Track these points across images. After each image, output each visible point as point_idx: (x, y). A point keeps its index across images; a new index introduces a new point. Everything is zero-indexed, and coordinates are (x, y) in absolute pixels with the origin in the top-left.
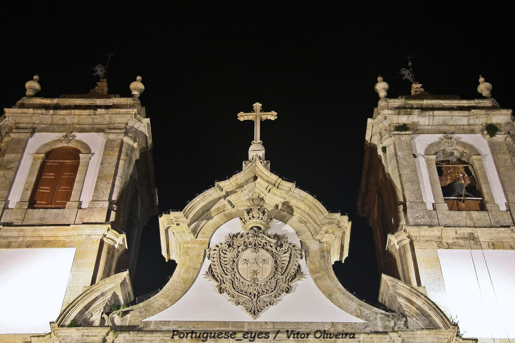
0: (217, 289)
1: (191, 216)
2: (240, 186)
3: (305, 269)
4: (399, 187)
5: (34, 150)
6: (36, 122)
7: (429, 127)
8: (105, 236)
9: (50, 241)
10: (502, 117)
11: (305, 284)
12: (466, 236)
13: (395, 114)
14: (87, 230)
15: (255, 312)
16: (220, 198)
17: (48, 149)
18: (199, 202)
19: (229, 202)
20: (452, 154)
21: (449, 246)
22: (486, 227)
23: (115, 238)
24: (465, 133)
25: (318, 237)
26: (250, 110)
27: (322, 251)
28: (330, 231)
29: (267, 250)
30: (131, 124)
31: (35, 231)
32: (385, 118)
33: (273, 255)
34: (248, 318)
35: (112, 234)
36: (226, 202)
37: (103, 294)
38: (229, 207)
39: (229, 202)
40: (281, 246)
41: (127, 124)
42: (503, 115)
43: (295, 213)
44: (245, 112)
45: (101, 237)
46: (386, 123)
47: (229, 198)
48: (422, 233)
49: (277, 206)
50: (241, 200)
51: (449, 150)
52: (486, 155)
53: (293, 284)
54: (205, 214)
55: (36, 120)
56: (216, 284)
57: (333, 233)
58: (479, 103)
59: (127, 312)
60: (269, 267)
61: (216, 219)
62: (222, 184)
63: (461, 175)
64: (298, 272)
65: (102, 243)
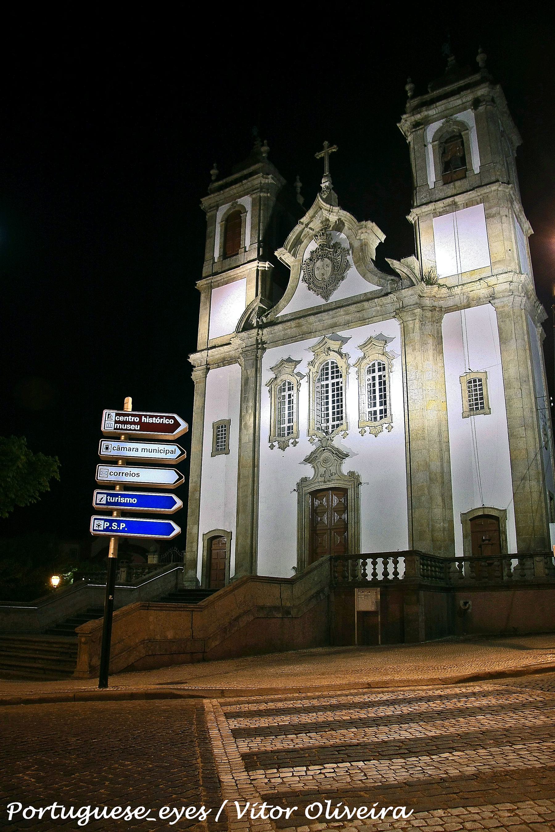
1: (288, 248)
2: (313, 216)
5: (220, 221)
6: (218, 200)
7: (436, 116)
8: (258, 266)
9: (234, 278)
10: (483, 90)
11: (352, 272)
12: (450, 203)
13: (411, 116)
14: (249, 266)
15: (326, 297)
16: (304, 229)
17: (226, 217)
18: (292, 236)
19: (310, 228)
20: (454, 131)
21: (441, 214)
22: (467, 191)
23: (264, 265)
24: (460, 112)
25: (358, 238)
26: (321, 149)
27: (362, 246)
28: (364, 231)
30: (263, 182)
31: (226, 274)
32: (406, 121)
34: (322, 302)
35: (261, 264)
36: (308, 229)
37: (253, 310)
39: (310, 228)
41: (261, 183)
42: (483, 88)
44: (319, 152)
45: (256, 268)
46: (408, 123)
47: (309, 226)
48: (424, 210)
49: (336, 222)
50: (316, 225)
51: (450, 130)
54: (298, 241)
55: (217, 199)
57: (366, 232)
58: (471, 79)
59: (268, 314)
61: (305, 241)
62: (302, 220)
64: (348, 266)
65: (258, 270)
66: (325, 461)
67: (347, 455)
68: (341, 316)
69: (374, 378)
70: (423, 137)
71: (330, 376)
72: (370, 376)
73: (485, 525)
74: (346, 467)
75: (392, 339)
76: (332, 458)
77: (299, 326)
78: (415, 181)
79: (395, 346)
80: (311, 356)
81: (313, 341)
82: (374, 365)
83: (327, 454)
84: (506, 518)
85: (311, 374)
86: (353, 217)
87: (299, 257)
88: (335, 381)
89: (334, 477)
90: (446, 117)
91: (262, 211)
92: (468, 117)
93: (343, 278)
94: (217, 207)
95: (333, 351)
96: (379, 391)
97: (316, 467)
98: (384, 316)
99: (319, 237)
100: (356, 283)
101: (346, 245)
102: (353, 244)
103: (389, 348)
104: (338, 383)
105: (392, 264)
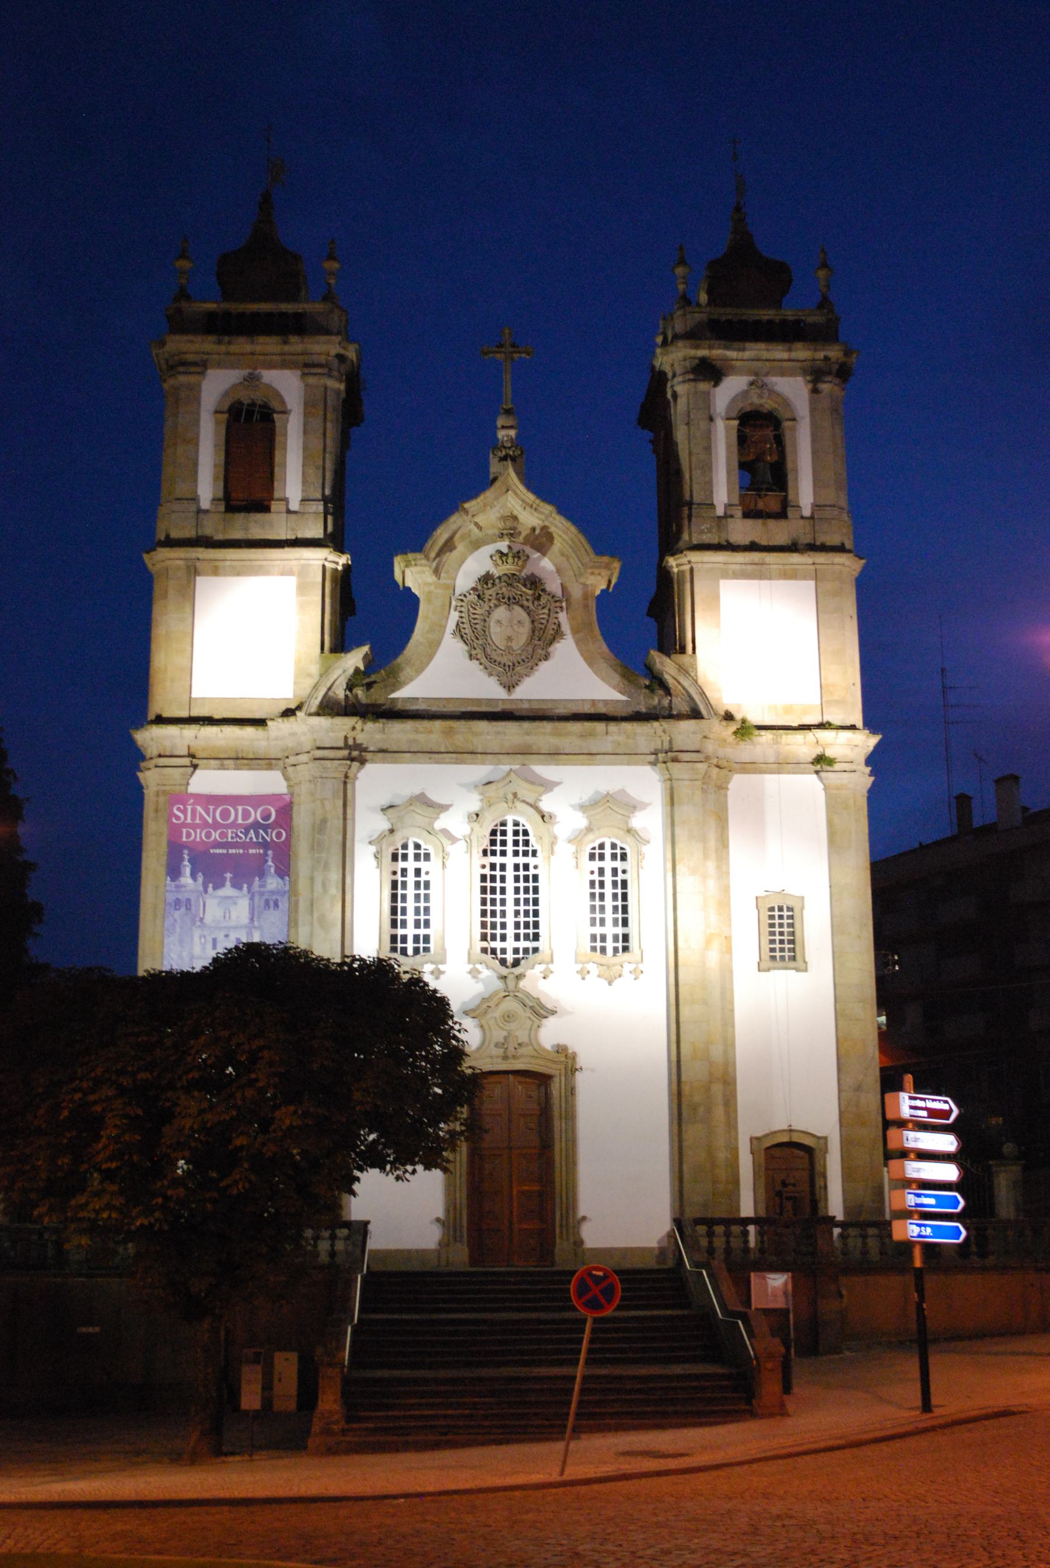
0: (467, 655)
3: (566, 627)
4: (687, 476)
9: (261, 566)
11: (566, 649)
15: (510, 687)
18: (442, 534)
19: (476, 524)
23: (336, 559)
25: (582, 580)
29: (522, 606)
33: (529, 614)
38: (476, 530)
39: (476, 524)
40: (539, 598)
43: (555, 542)
45: (321, 563)
52: (804, 418)
53: (551, 649)
56: (466, 648)
60: (525, 631)
63: (768, 446)
64: (558, 634)
65: (324, 566)
66: (508, 1017)
67: (553, 1013)
68: (542, 734)
69: (601, 871)
70: (707, 400)
71: (510, 848)
72: (596, 864)
73: (790, 1160)
74: (550, 1034)
75: (644, 806)
76: (524, 1014)
77: (449, 733)
78: (687, 488)
79: (651, 821)
80: (474, 803)
81: (480, 771)
82: (602, 846)
83: (510, 1005)
84: (826, 1151)
85: (474, 838)
86: (583, 540)
87: (444, 580)
88: (521, 860)
89: (521, 1051)
90: (756, 374)
91: (329, 425)
92: (793, 390)
93: (546, 657)
94: (202, 366)
95: (524, 801)
96: (613, 896)
97: (486, 1027)
98: (628, 755)
99: (510, 560)
100: (573, 674)
101: (554, 586)
102: (570, 590)
103: (637, 821)
104: (526, 867)
105: (661, 663)
